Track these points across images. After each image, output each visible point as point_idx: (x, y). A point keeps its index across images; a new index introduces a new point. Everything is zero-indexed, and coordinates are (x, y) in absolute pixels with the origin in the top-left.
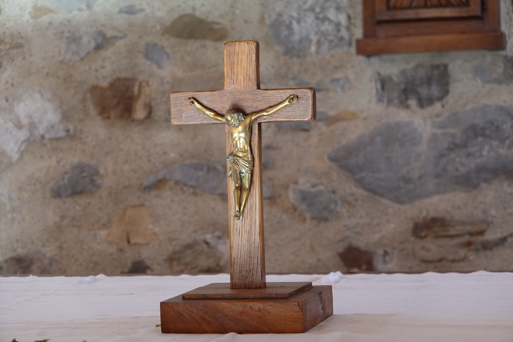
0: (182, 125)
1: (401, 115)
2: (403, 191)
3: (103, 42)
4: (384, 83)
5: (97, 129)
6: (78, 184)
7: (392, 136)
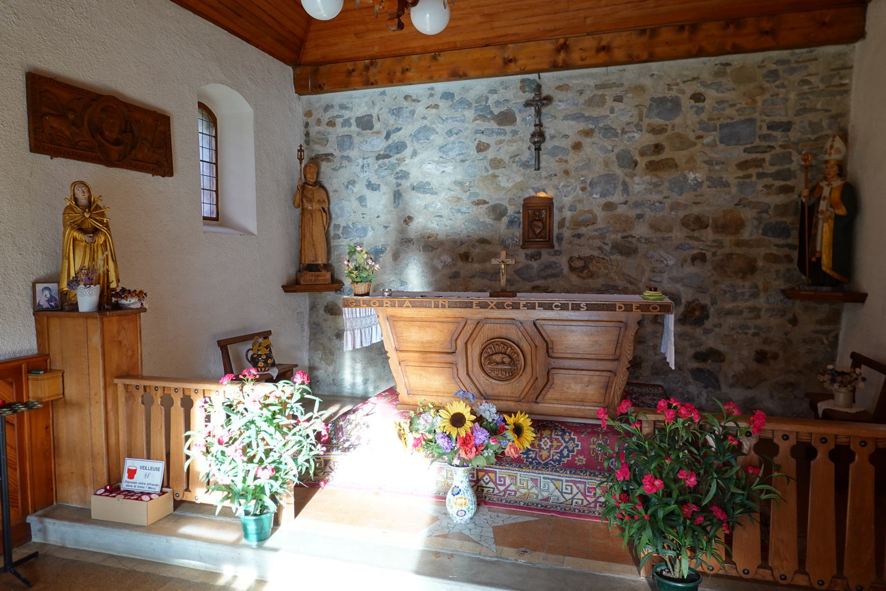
0: (309, 323)
1: (530, 262)
2: (530, 279)
3: (462, 243)
4: (527, 255)
5: (460, 263)
6: (455, 276)
7: (528, 267)
